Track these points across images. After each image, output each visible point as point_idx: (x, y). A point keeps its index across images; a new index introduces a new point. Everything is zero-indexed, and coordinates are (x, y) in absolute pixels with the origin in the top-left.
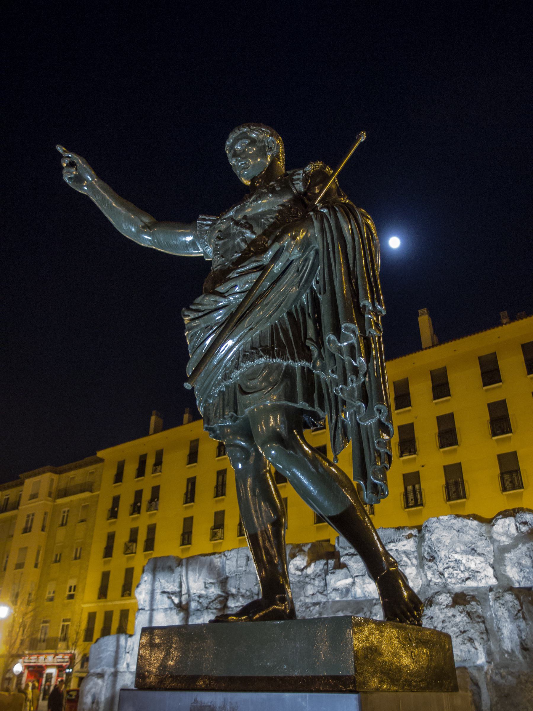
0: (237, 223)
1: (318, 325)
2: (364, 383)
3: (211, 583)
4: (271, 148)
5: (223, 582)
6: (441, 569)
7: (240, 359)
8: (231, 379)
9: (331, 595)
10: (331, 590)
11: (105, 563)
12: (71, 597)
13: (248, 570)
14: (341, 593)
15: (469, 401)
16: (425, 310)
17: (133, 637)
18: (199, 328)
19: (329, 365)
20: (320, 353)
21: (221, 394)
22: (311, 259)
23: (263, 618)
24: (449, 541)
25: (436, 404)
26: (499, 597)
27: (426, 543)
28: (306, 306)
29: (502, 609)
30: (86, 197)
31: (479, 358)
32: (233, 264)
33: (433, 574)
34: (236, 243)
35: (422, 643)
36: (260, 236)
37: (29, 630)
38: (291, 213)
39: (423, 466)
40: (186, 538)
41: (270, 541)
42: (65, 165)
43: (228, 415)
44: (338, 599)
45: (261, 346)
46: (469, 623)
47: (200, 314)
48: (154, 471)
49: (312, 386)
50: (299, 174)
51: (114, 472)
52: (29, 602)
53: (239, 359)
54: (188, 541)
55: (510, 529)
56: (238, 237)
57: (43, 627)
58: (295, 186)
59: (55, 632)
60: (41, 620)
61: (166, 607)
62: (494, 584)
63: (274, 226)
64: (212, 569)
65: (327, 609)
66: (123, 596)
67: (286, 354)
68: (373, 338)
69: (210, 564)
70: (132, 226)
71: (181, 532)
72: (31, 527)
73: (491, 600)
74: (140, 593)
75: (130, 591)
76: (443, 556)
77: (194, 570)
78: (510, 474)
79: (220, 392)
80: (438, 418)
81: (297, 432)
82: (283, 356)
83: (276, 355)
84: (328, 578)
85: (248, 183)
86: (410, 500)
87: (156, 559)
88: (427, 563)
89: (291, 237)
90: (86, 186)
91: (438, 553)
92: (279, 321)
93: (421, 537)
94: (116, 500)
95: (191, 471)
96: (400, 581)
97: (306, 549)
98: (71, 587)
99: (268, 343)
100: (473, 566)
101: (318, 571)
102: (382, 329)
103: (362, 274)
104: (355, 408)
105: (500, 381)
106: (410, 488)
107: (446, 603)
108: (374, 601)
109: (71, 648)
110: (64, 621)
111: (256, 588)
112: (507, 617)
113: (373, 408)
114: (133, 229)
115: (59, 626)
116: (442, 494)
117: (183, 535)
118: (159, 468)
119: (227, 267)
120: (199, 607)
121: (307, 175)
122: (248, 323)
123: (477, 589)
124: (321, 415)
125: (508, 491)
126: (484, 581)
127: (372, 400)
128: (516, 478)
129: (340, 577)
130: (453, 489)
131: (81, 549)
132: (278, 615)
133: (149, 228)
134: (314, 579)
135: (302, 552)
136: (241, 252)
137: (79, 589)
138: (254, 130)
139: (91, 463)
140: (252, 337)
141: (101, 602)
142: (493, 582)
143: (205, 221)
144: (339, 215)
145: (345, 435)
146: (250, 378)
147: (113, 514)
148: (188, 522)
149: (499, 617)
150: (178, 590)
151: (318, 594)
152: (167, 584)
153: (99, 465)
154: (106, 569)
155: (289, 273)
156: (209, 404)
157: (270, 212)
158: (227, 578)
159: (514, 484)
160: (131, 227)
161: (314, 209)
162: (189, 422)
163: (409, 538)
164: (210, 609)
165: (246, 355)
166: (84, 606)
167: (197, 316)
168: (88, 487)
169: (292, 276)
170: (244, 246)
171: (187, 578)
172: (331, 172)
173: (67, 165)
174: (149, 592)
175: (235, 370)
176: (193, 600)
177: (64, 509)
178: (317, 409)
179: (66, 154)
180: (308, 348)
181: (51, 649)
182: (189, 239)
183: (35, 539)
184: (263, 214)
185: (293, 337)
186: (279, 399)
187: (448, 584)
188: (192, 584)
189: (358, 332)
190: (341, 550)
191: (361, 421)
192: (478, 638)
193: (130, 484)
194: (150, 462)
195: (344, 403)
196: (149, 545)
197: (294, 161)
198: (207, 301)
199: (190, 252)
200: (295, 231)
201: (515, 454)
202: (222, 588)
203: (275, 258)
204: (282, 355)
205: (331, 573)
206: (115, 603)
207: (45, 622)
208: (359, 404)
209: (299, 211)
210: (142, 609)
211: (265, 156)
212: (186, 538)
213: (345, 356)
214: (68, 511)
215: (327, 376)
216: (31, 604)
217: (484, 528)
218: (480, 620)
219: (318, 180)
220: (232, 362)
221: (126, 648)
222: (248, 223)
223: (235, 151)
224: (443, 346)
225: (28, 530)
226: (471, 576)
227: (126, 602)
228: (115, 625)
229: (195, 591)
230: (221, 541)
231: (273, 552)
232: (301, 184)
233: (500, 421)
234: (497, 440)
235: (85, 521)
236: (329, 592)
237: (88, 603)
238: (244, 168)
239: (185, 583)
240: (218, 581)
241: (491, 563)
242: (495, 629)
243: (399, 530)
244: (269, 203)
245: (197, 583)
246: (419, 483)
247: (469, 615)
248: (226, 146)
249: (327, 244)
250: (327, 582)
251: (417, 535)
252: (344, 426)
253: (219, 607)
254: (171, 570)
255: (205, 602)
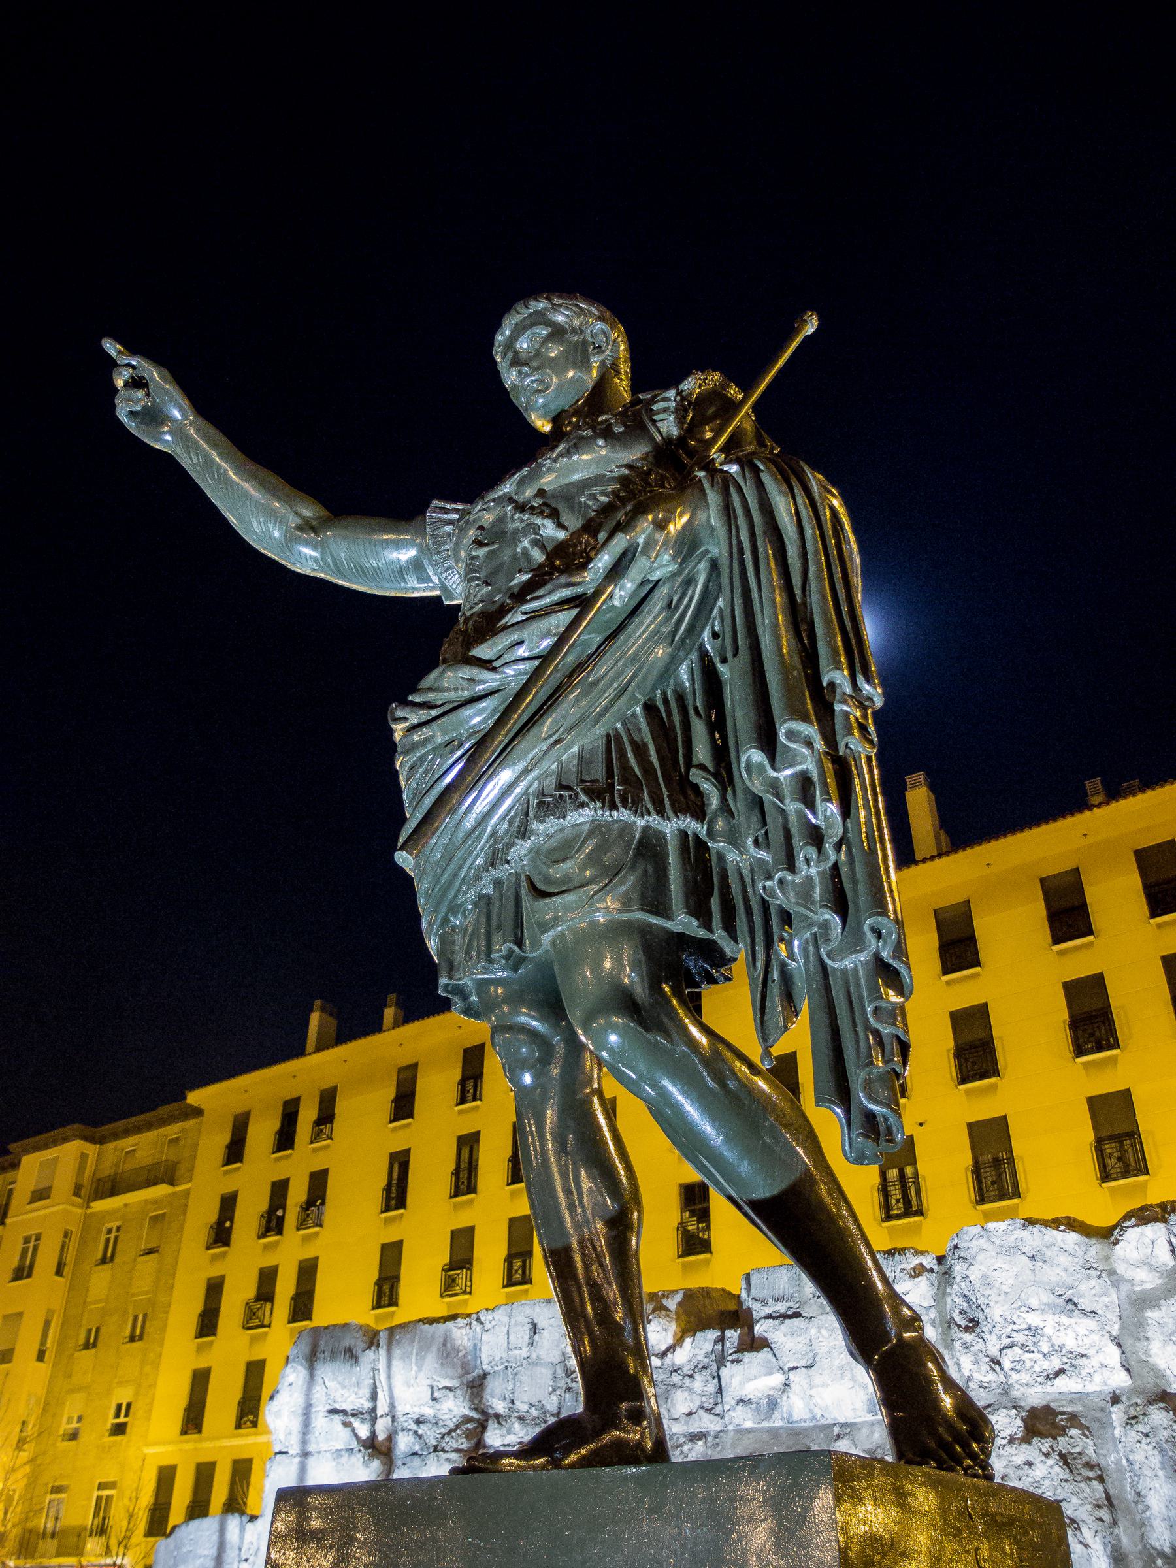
0: (521, 507)
1: (717, 736)
2: (835, 866)
3: (446, 1388)
4: (599, 347)
5: (476, 1386)
6: (994, 1351)
7: (531, 814)
8: (508, 862)
9: (732, 1413)
10: (733, 1403)
11: (200, 1349)
12: (119, 1429)
13: (534, 1356)
14: (758, 1410)
15: (1021, 977)
16: (920, 776)
17: (259, 1522)
18: (429, 747)
19: (749, 827)
20: (724, 799)
21: (482, 904)
22: (701, 580)
23: (585, 1463)
24: (1011, 1281)
25: (948, 983)
26: (1135, 1417)
27: (955, 1286)
28: (689, 692)
29: (1144, 1446)
30: (168, 461)
31: (1043, 881)
32: (512, 596)
33: (976, 1363)
34: (519, 550)
35: (998, 1526)
36: (577, 534)
37: (19, 1509)
38: (649, 484)
39: (921, 1125)
40: (387, 1290)
41: (601, 1265)
42: (120, 383)
43: (500, 951)
44: (749, 1424)
45: (583, 781)
46: (1066, 1481)
47: (434, 713)
48: (316, 1137)
49: (705, 880)
50: (667, 399)
51: (225, 1138)
52: (21, 1443)
53: (527, 814)
54: (391, 1298)
55: (1156, 1251)
56: (525, 536)
57: (50, 1501)
58: (658, 424)
59: (78, 1512)
60: (47, 1485)
61: (340, 1446)
62: (1123, 1385)
63: (607, 510)
64: (448, 1354)
65: (723, 1449)
66: (238, 1426)
67: (642, 800)
68: (855, 760)
69: (445, 1345)
70: (268, 522)
71: (375, 1277)
72: (31, 1267)
73: (1115, 1424)
74: (278, 1414)
75: (257, 1416)
76: (998, 1319)
77: (406, 1357)
78: (1117, 1140)
79: (481, 897)
80: (953, 1015)
81: (672, 988)
82: (635, 806)
83: (618, 801)
84: (724, 1372)
85: (545, 426)
86: (894, 1202)
87: (316, 1331)
88: (960, 1335)
89: (653, 522)
90: (169, 432)
91: (987, 1310)
92: (624, 723)
93: (945, 1273)
94: (228, 1204)
95: (399, 1137)
96: (930, 1365)
97: (672, 1304)
98: (119, 1407)
99: (600, 773)
100: (1071, 1344)
101: (700, 1357)
102: (876, 740)
103: (825, 613)
104: (815, 929)
105: (1090, 932)
106: (893, 1174)
107: (1009, 1432)
108: (836, 1430)
109: (114, 1553)
110: (101, 1486)
111: (554, 1398)
112: (1158, 1465)
113: (860, 925)
114: (277, 534)
115: (89, 1499)
116: (965, 1188)
117: (379, 1284)
118: (326, 1129)
119: (497, 606)
120: (417, 1448)
121: (683, 397)
122: (550, 728)
123: (1081, 1396)
124: (728, 950)
125: (1115, 1179)
126: (1097, 1378)
127: (857, 905)
128: (1130, 1151)
129: (753, 1372)
130: (989, 1175)
131: (145, 1316)
132: (626, 1455)
133: (314, 529)
134: (691, 1376)
135: (663, 1312)
136: (532, 571)
137: (138, 1410)
138: (560, 305)
139: (172, 1119)
140: (558, 759)
141: (188, 1441)
142: (1120, 1380)
143: (442, 514)
144: (766, 478)
145: (789, 996)
146: (554, 858)
147: (221, 1235)
148: (391, 1254)
149: (1137, 1466)
150: (368, 1405)
151: (701, 1412)
152: (341, 1391)
153: (192, 1123)
154: (202, 1364)
155: (649, 612)
156: (453, 929)
157: (599, 480)
158: (485, 1375)
159: (1127, 1165)
160: (271, 527)
161: (709, 467)
162: (396, 1025)
163: (916, 1276)
164: (443, 1450)
165: (548, 804)
166: (147, 1450)
167: (425, 718)
168: (166, 1174)
169: (656, 617)
170: (538, 556)
171: (389, 1377)
172: (740, 397)
173: (126, 384)
174: (300, 1411)
175: (518, 841)
176: (403, 1430)
177: (109, 1225)
178: (719, 935)
179: (125, 360)
180: (696, 788)
181: (69, 1555)
182: (406, 555)
183: (43, 1293)
184: (583, 485)
185: (661, 760)
186: (626, 906)
187: (1010, 1386)
188: (401, 1392)
189: (819, 745)
190: (755, 1306)
191: (833, 960)
192: (1090, 1520)
193: (261, 1166)
194: (307, 1116)
195: (787, 918)
196: (302, 1307)
197: (652, 372)
198: (450, 681)
199: (410, 585)
200: (664, 511)
201: (1126, 1095)
202: (471, 1401)
203: (616, 572)
204: (633, 803)
205: (733, 1361)
206: (221, 1442)
207: (58, 1490)
208: (827, 916)
209: (671, 472)
210: (281, 1453)
211: (585, 364)
212: (387, 1290)
213: (787, 801)
214: (118, 1229)
215: (741, 856)
216: (26, 1447)
217: (1095, 1249)
218: (1091, 1474)
219: (711, 411)
220: (511, 822)
221: (240, 1549)
222: (549, 507)
223: (516, 353)
224: (961, 855)
225: (25, 1274)
226: (1065, 1367)
227: (245, 1443)
228: (219, 1494)
229: (408, 1409)
230: (467, 1296)
231: (612, 1294)
232: (672, 418)
233: (1092, 1021)
234: (1086, 1065)
235: (157, 1251)
236: (727, 1407)
237: (155, 1444)
238: (537, 392)
239: (386, 1387)
240: (462, 1382)
241: (1114, 1333)
242: (1131, 1497)
243: (893, 1255)
244: (598, 461)
245: (414, 1390)
246: (914, 1163)
247: (1066, 1463)
248: (496, 345)
249: (740, 542)
250: (723, 1384)
251: (935, 1268)
252: (786, 978)
253: (465, 1446)
254: (351, 1355)
255: (431, 1435)
